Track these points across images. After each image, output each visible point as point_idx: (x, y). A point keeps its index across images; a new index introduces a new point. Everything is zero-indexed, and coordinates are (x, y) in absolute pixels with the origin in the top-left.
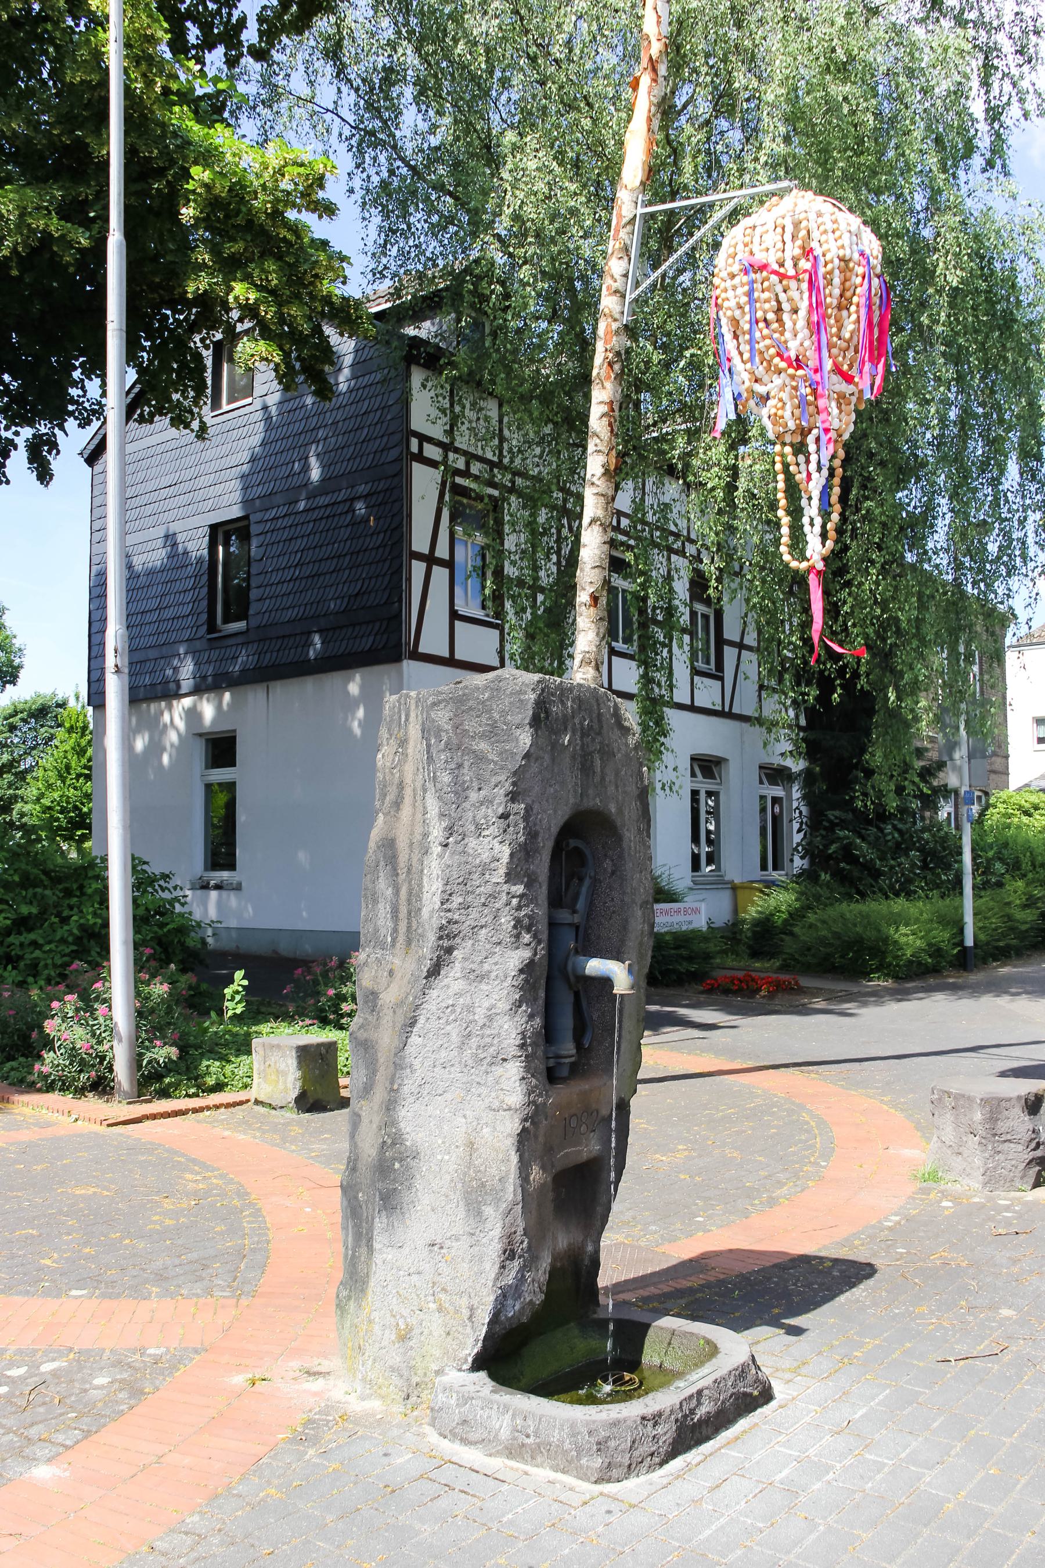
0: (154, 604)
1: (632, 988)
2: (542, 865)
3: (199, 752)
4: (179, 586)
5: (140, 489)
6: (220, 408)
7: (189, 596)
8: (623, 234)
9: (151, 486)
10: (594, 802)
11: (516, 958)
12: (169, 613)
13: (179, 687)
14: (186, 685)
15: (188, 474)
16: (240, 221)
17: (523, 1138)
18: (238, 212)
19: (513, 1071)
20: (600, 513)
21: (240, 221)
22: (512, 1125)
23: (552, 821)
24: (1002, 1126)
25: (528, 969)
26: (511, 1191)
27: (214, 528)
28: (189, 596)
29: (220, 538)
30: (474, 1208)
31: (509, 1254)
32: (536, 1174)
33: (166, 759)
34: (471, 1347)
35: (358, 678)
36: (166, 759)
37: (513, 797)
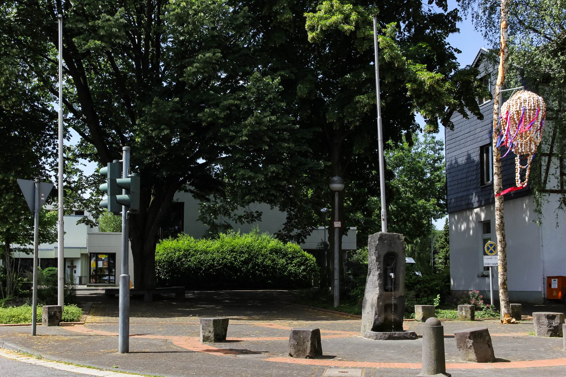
0: (465, 175)
1: (168, 238)
2: (382, 259)
3: (481, 231)
4: (472, 169)
5: (459, 134)
6: (482, 103)
7: (475, 173)
8: (497, 98)
9: (462, 133)
10: (392, 250)
11: (378, 273)
12: (470, 179)
13: (473, 205)
14: (476, 204)
15: (473, 128)
16: (422, 92)
17: (378, 298)
18: (421, 90)
19: (378, 288)
20: (496, 171)
21: (422, 92)
22: (377, 296)
23: (383, 253)
24: (541, 321)
25: (379, 274)
26: (376, 305)
27: (481, 147)
28: (475, 173)
29: (485, 151)
30: (372, 308)
31: (376, 314)
32: (381, 303)
33: (471, 232)
34: (371, 327)
35: (527, 201)
36: (471, 232)
37: (376, 250)
